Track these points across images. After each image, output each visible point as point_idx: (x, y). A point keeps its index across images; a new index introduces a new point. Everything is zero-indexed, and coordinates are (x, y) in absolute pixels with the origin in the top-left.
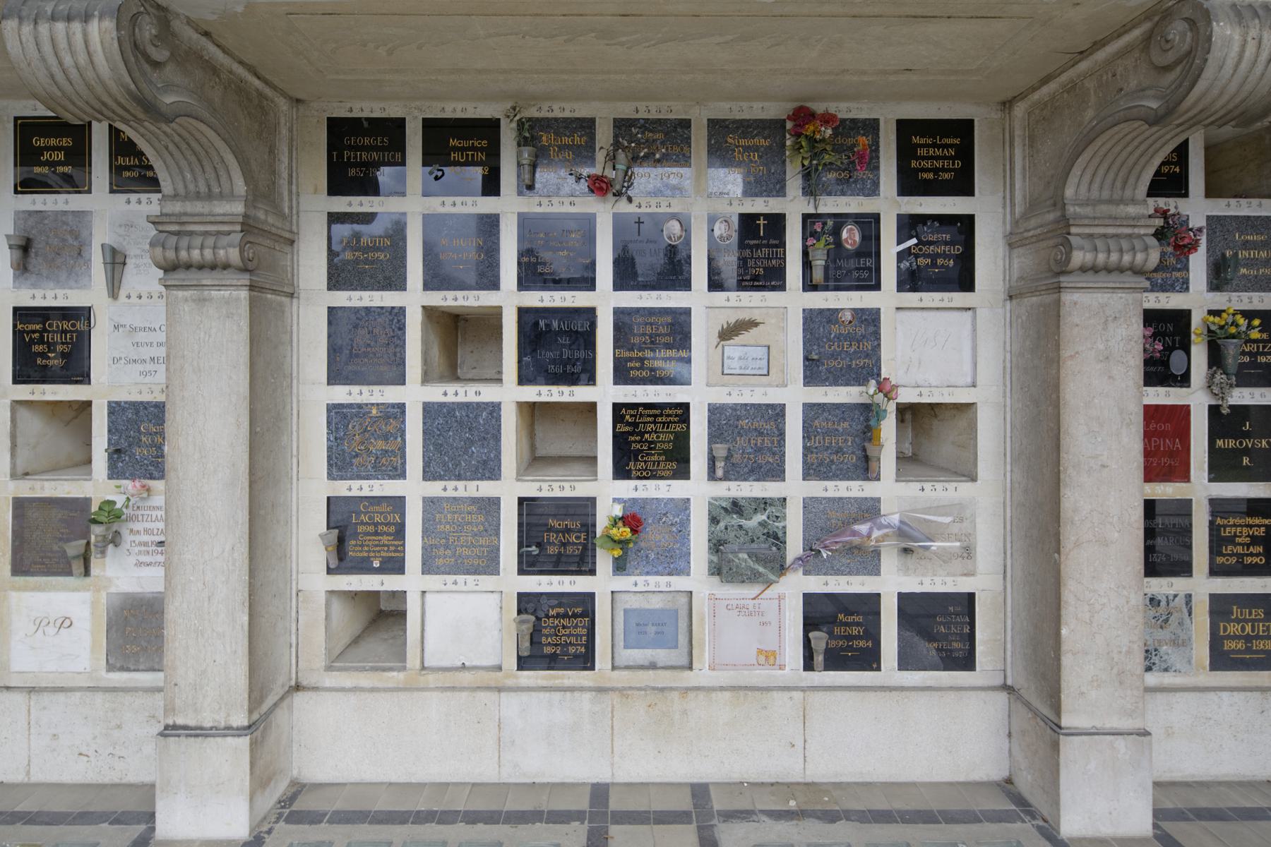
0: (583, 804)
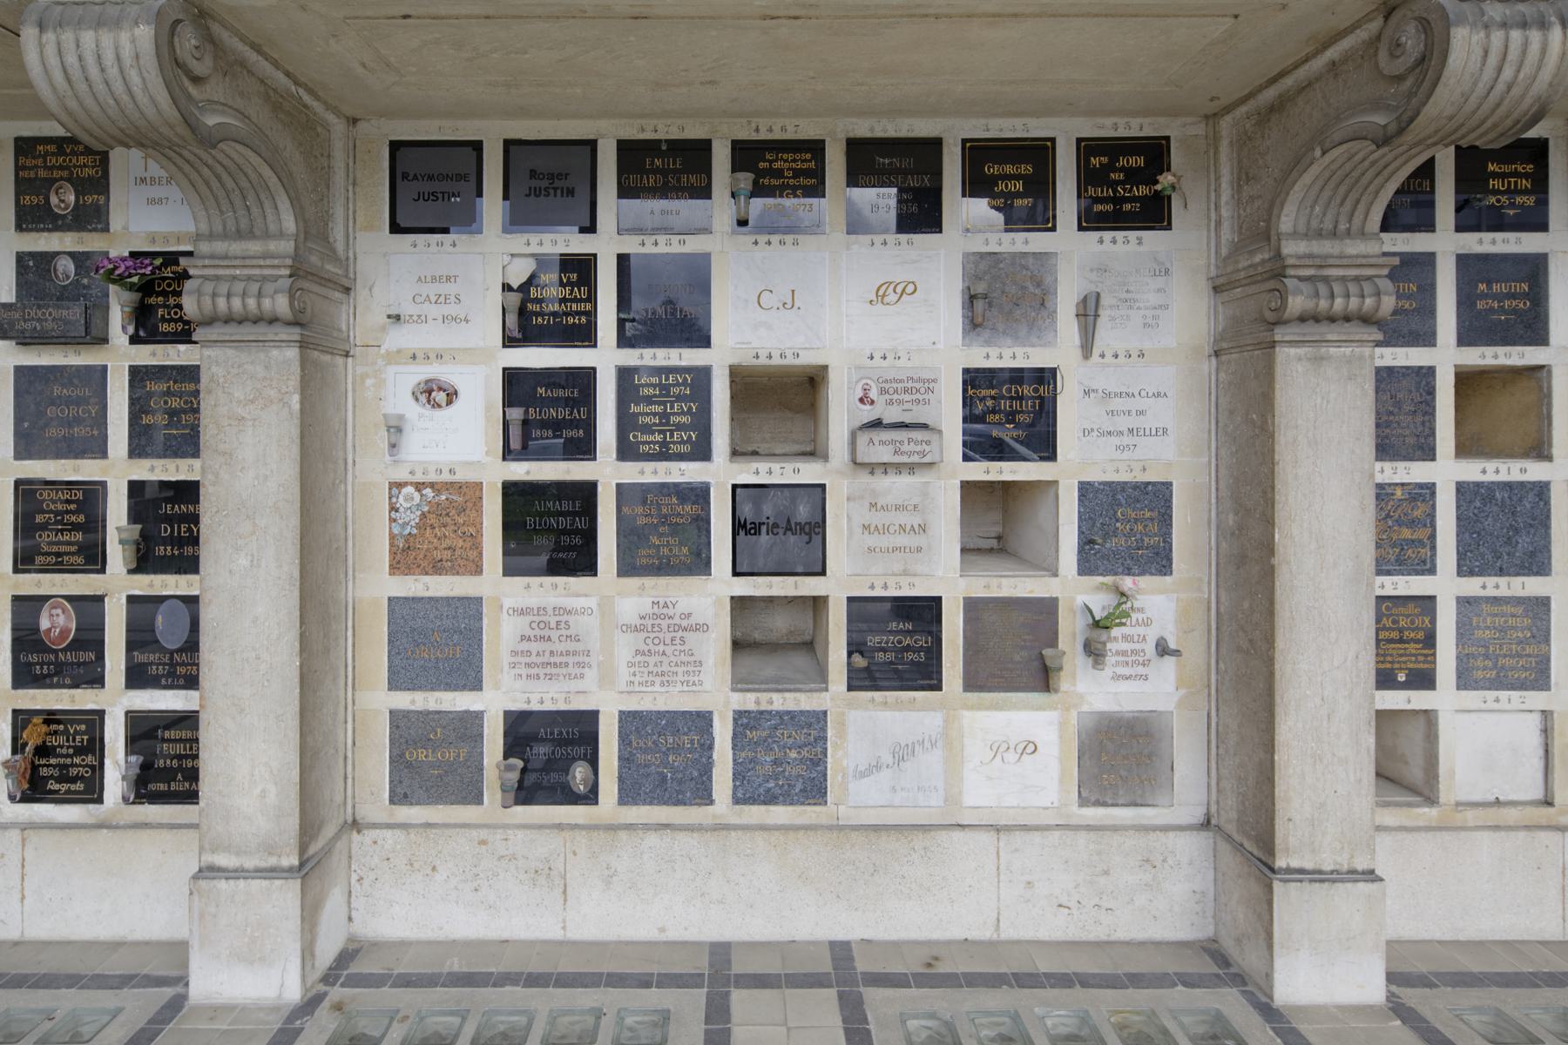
0: (826, 966)
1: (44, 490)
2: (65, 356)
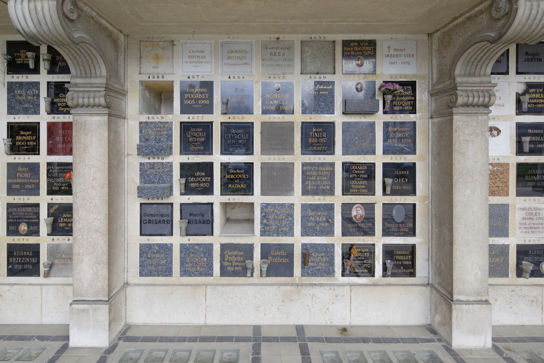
0: (294, 334)
1: (353, 166)
2: (360, 118)
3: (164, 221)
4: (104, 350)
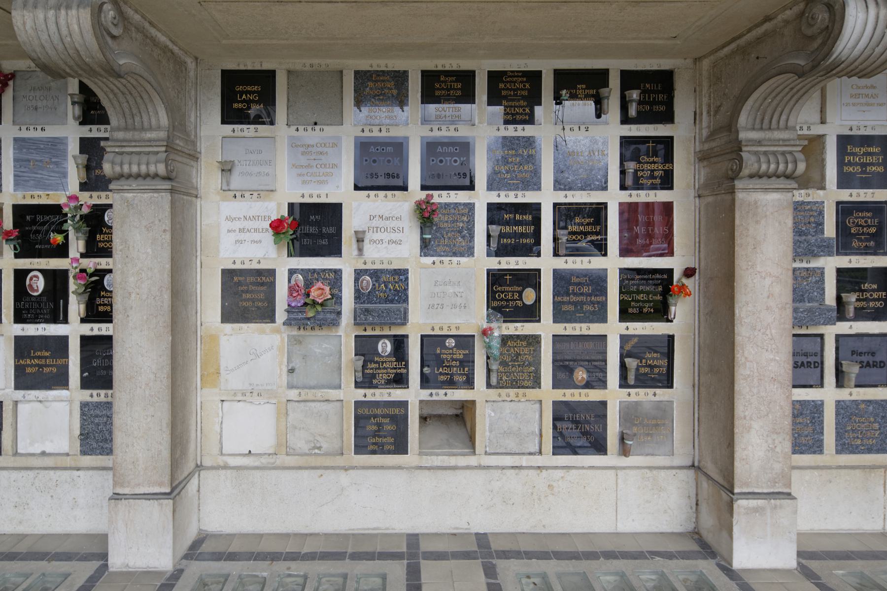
3: (809, 364)
4: (168, 575)
